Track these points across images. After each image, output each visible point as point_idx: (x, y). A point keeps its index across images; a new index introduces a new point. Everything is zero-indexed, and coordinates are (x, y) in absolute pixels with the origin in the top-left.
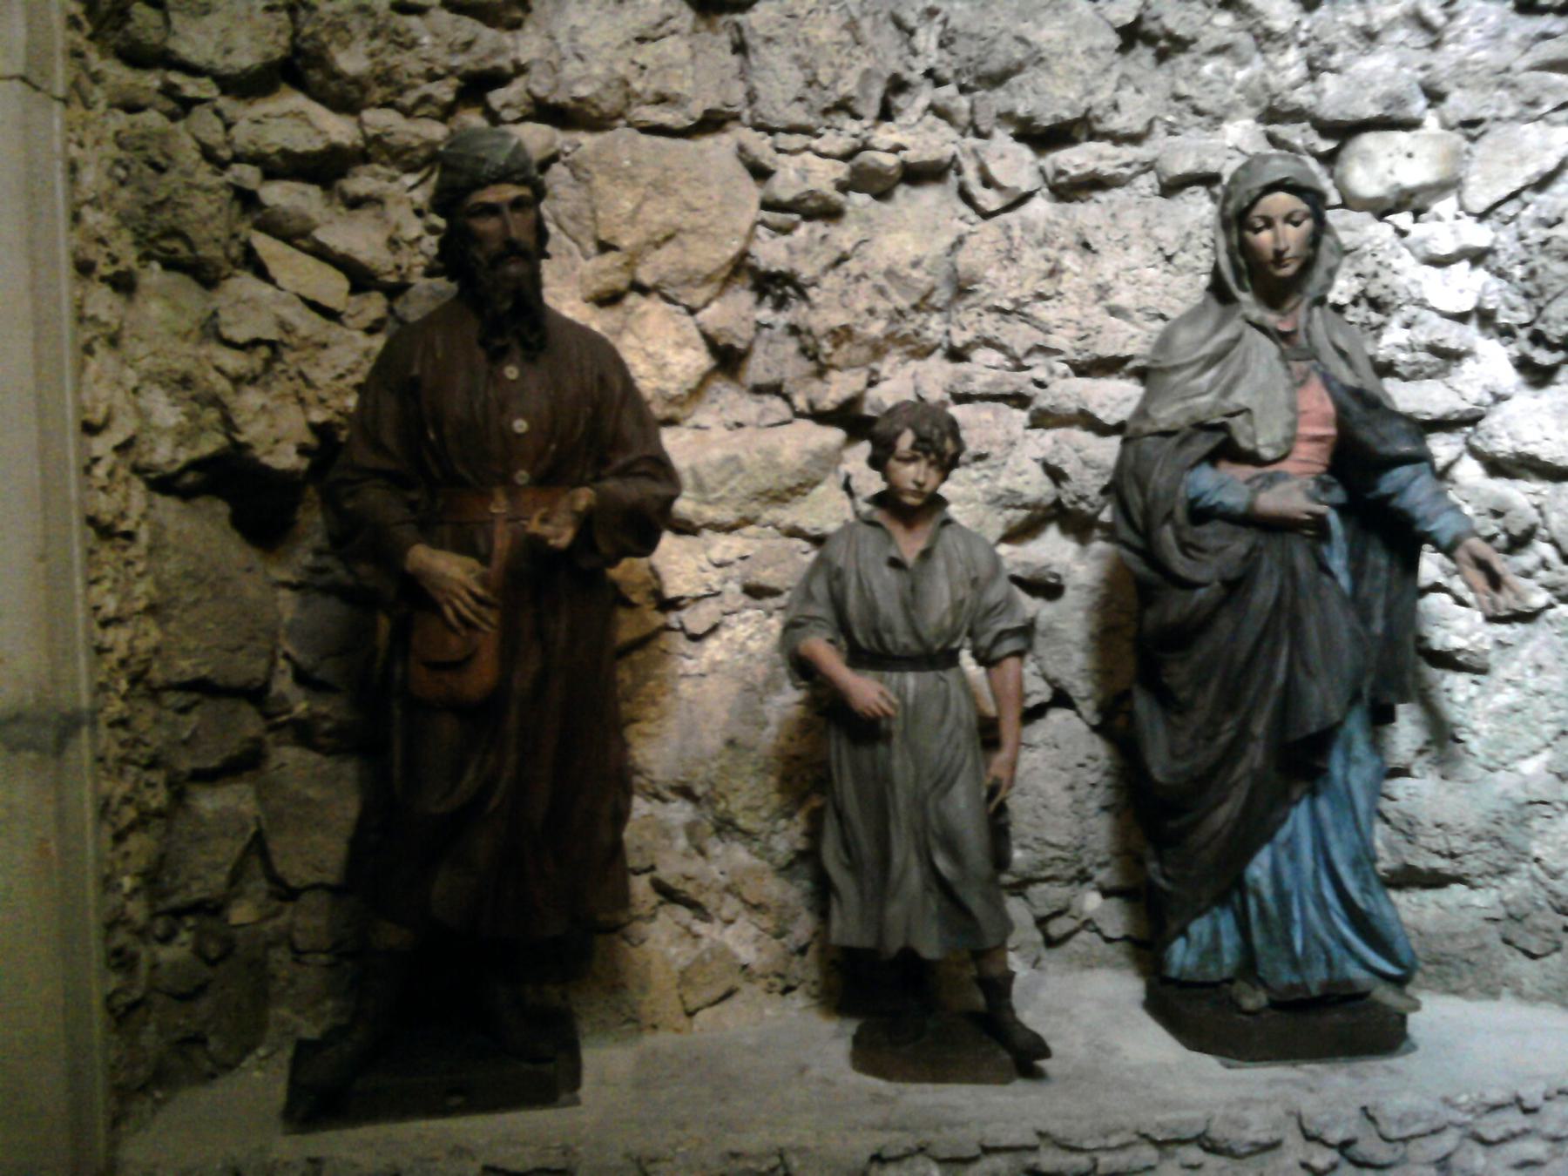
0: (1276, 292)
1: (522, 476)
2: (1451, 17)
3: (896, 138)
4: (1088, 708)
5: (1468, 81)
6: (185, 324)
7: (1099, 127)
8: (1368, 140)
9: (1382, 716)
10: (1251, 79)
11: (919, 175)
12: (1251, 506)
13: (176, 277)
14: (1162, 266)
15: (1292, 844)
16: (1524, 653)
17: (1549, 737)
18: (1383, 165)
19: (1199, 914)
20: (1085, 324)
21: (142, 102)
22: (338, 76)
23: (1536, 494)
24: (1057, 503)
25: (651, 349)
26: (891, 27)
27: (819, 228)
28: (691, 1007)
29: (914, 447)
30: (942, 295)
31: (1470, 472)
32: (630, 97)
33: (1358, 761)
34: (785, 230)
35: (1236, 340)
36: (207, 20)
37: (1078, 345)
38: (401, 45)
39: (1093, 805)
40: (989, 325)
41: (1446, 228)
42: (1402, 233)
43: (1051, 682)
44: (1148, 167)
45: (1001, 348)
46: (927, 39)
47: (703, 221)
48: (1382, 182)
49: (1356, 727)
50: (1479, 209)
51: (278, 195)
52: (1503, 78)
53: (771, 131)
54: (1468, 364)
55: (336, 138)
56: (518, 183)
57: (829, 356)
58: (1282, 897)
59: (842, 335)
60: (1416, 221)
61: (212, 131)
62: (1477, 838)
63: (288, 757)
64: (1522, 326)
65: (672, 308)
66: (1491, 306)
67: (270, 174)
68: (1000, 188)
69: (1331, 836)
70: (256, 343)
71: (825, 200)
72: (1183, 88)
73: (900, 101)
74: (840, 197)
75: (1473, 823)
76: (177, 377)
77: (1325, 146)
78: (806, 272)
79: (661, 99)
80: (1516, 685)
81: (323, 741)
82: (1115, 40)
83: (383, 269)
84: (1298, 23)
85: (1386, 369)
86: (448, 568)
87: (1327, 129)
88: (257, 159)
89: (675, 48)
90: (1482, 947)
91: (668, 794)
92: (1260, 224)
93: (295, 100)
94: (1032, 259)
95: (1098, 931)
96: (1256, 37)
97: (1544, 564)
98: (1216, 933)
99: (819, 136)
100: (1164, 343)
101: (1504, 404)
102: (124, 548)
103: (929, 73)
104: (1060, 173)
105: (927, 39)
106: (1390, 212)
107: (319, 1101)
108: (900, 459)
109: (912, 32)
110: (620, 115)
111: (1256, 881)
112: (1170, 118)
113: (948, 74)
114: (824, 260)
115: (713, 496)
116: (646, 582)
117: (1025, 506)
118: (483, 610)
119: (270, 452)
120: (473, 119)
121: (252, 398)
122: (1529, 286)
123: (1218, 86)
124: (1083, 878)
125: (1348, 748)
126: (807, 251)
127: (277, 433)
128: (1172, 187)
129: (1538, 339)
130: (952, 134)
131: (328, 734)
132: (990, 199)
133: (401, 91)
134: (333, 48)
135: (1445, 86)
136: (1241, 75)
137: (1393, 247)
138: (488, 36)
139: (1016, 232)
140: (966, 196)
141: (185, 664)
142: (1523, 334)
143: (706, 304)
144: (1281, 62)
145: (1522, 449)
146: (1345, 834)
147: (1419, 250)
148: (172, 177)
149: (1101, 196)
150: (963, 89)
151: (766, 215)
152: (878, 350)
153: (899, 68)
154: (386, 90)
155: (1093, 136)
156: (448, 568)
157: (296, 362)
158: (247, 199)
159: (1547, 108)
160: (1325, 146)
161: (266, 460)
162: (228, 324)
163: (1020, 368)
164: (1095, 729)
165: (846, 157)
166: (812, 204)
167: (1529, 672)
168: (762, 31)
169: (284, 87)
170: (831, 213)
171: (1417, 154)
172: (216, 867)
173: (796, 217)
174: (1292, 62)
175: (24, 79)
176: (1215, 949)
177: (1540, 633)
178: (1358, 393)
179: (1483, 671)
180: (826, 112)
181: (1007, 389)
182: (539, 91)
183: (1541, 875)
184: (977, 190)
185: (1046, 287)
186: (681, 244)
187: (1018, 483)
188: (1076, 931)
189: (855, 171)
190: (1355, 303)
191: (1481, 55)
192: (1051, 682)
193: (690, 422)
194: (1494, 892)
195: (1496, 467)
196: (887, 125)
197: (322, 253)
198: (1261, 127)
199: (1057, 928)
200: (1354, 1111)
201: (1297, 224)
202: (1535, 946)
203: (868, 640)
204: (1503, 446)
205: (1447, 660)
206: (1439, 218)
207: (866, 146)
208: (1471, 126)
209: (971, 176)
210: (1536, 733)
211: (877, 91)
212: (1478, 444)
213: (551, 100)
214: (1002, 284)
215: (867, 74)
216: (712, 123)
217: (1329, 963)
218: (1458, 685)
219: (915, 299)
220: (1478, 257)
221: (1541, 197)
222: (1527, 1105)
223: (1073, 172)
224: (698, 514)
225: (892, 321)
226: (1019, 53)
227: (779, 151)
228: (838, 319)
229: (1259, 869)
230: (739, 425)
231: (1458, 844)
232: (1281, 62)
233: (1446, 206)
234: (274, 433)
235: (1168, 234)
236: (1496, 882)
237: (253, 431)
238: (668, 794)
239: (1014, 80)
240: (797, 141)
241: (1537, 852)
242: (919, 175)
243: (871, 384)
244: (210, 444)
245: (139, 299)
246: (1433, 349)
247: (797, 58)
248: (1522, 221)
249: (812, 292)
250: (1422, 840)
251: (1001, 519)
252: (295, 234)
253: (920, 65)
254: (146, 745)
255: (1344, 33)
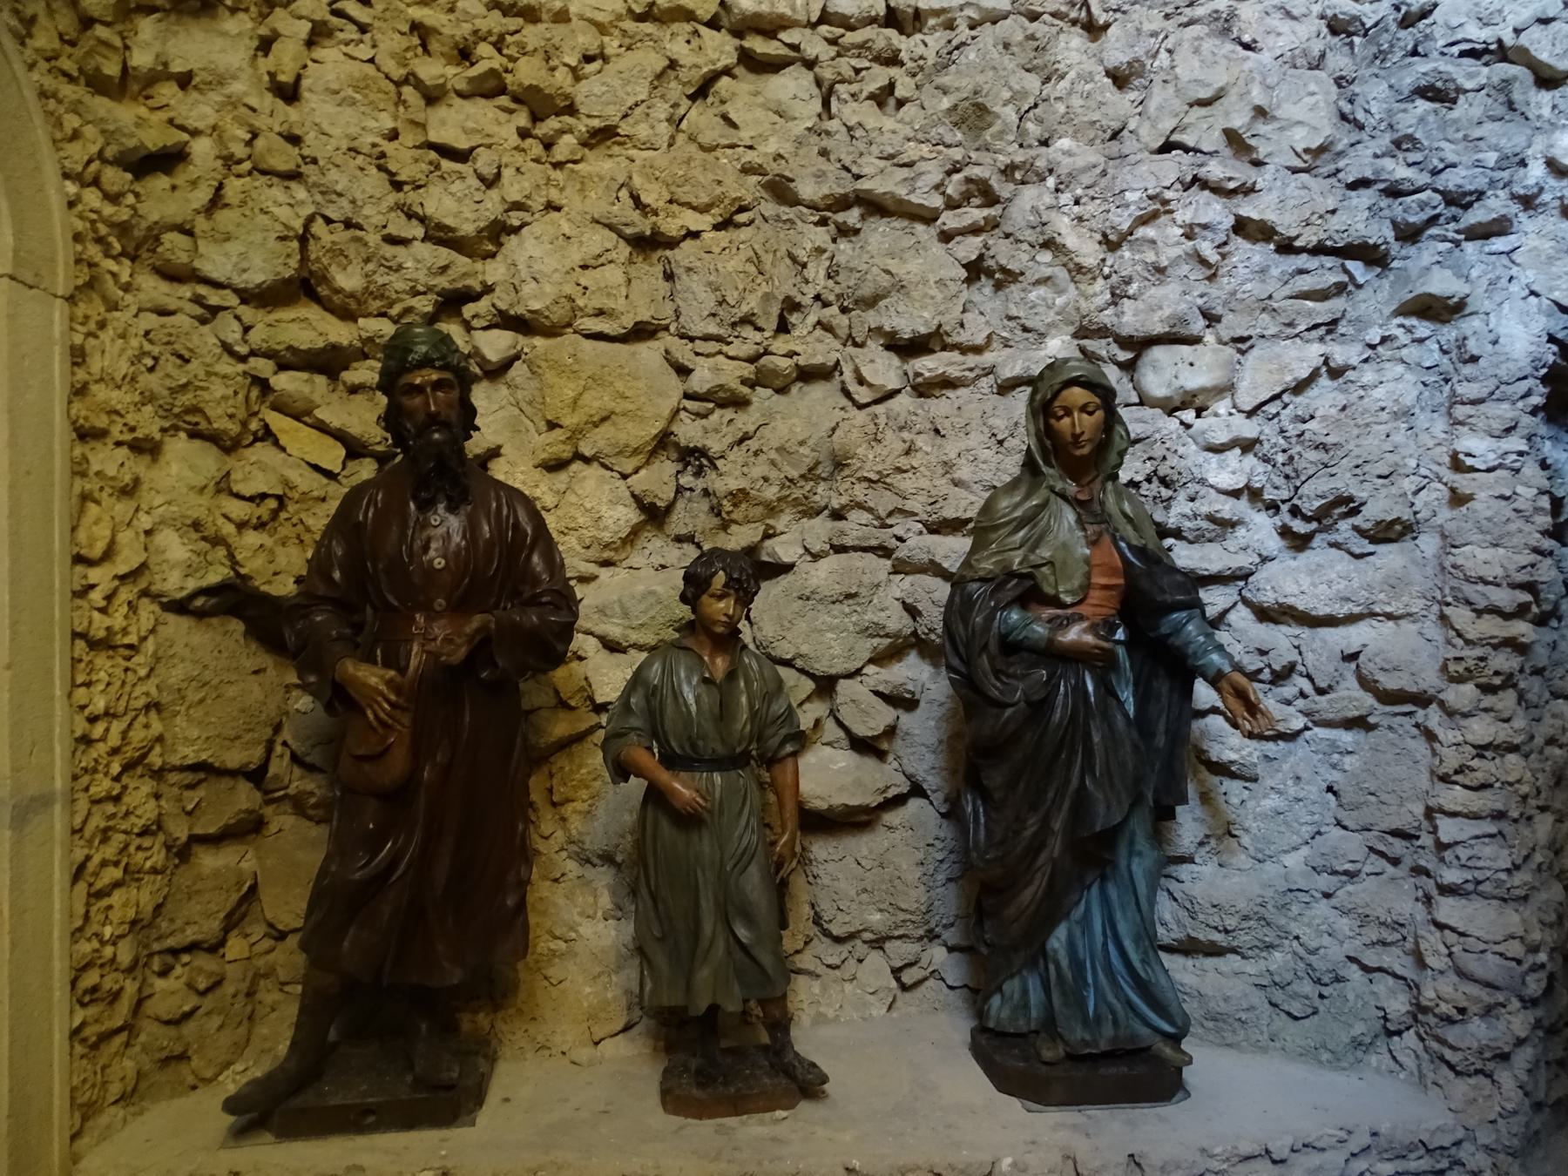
0: (1076, 469)
1: (440, 603)
2: (1224, 256)
3: (793, 347)
4: (937, 798)
5: (1238, 307)
6: (199, 481)
7: (949, 340)
8: (1158, 353)
9: (1165, 814)
10: (1067, 304)
11: (809, 375)
12: (1051, 641)
13: (197, 443)
14: (995, 448)
15: (1086, 919)
16: (1286, 767)
17: (1307, 836)
18: (1169, 372)
19: (1012, 976)
20: (933, 493)
21: (172, 307)
22: (338, 291)
23: (1297, 637)
24: (915, 634)
25: (588, 506)
26: (788, 261)
27: (729, 413)
28: (597, 1039)
29: (726, 585)
30: (823, 470)
31: (1241, 617)
32: (575, 311)
33: (1140, 854)
34: (703, 416)
35: (1044, 505)
36: (227, 245)
37: (929, 508)
38: (390, 268)
39: (941, 877)
40: (860, 491)
41: (1222, 422)
42: (1188, 426)
43: (909, 777)
44: (990, 371)
45: (870, 510)
46: (817, 271)
47: (632, 407)
48: (1169, 385)
49: (1140, 827)
50: (1248, 408)
51: (285, 382)
52: (1265, 305)
53: (692, 339)
54: (1241, 532)
55: (333, 339)
56: (441, 368)
57: (728, 513)
58: (1077, 965)
59: (739, 497)
60: (1198, 416)
61: (232, 333)
62: (1246, 918)
63: (282, 821)
64: (1284, 502)
65: (609, 473)
66: (1258, 485)
67: (283, 367)
68: (870, 385)
69: (1118, 915)
70: (263, 496)
71: (732, 391)
72: (1014, 312)
73: (794, 318)
74: (745, 390)
75: (1242, 905)
76: (189, 522)
77: (1124, 356)
78: (715, 445)
79: (600, 313)
80: (1279, 792)
81: (311, 812)
82: (963, 274)
83: (372, 440)
84: (1104, 260)
85: (1163, 532)
86: (372, 677)
87: (1125, 342)
88: (269, 354)
89: (613, 275)
90: (1251, 1008)
91: (595, 860)
92: (1061, 413)
93: (312, 312)
94: (893, 442)
95: (943, 979)
96: (1070, 271)
97: (1303, 695)
98: (1025, 992)
99: (729, 343)
100: (987, 508)
101: (1269, 564)
102: (128, 659)
103: (817, 297)
104: (918, 374)
105: (817, 271)
106: (1177, 409)
107: (265, 1112)
108: (712, 596)
109: (804, 266)
110: (569, 325)
111: (1055, 951)
112: (1004, 334)
113: (832, 298)
114: (729, 439)
115: (636, 623)
116: (582, 689)
117: (887, 636)
118: (398, 713)
119: (269, 582)
120: (452, 329)
121: (252, 538)
122: (1288, 470)
123: (1040, 309)
124: (931, 936)
125: (1132, 843)
126: (717, 431)
127: (279, 566)
128: (1005, 388)
129: (1295, 512)
130: (837, 344)
131: (315, 806)
132: (863, 394)
133: (391, 306)
134: (333, 269)
135: (1219, 310)
136: (1059, 301)
137: (1179, 437)
138: (462, 262)
139: (882, 420)
140: (847, 394)
141: (187, 751)
142: (1285, 508)
143: (636, 472)
144: (1090, 290)
145: (1281, 600)
146: (1129, 914)
147: (1200, 440)
148: (194, 366)
149: (950, 393)
150: (844, 310)
151: (688, 404)
152: (772, 509)
153: (793, 293)
154: (378, 303)
155: (945, 347)
156: (372, 677)
157: (297, 512)
158: (264, 385)
159: (1302, 328)
160: (1124, 356)
161: (264, 588)
162: (236, 481)
163: (885, 526)
164: (943, 815)
165: (752, 360)
166: (721, 394)
167: (1290, 783)
168: (686, 263)
169: (304, 299)
170: (740, 403)
171: (1197, 364)
172: (210, 915)
173: (711, 405)
174: (1100, 290)
175: (12, 278)
176: (1025, 1005)
177: (1300, 749)
178: (1141, 552)
179: (1255, 780)
180: (734, 325)
181: (874, 543)
182: (502, 306)
183: (1301, 951)
184: (853, 387)
185: (904, 462)
186: (614, 424)
187: (880, 617)
188: (926, 979)
189: (758, 371)
190: (1149, 480)
191: (1248, 286)
192: (909, 777)
193: (624, 564)
194: (1262, 961)
195: (1264, 614)
196: (783, 337)
197: (322, 427)
198: (1076, 342)
199: (908, 977)
200: (1123, 1159)
201: (1091, 414)
202: (1296, 1008)
203: (682, 748)
204: (1268, 598)
205: (1223, 769)
206: (1216, 415)
207: (767, 352)
208: (1241, 342)
209: (848, 375)
210: (1297, 833)
211: (775, 310)
212: (1249, 595)
213: (512, 312)
214: (870, 460)
215: (767, 297)
216: (642, 332)
217: (1115, 1022)
218: (1233, 787)
219: (804, 471)
220: (1248, 446)
221: (1299, 399)
222: (1275, 1157)
223: (927, 374)
224: (625, 637)
225: (783, 487)
226: (885, 281)
227: (697, 354)
228: (734, 484)
229: (1058, 941)
230: (663, 567)
231: (1231, 922)
232: (1090, 290)
233: (1222, 407)
234: (272, 568)
235: (1000, 424)
236: (1264, 954)
237: (252, 565)
238: (595, 860)
239: (882, 303)
240: (712, 346)
241: (1297, 931)
242: (809, 375)
243: (767, 536)
244: (216, 575)
245: (163, 460)
246: (1211, 518)
247: (710, 284)
248: (1282, 417)
249: (719, 463)
250: (1201, 917)
251: (868, 645)
252: (300, 413)
253: (811, 291)
254: (139, 817)
255: (1138, 268)
